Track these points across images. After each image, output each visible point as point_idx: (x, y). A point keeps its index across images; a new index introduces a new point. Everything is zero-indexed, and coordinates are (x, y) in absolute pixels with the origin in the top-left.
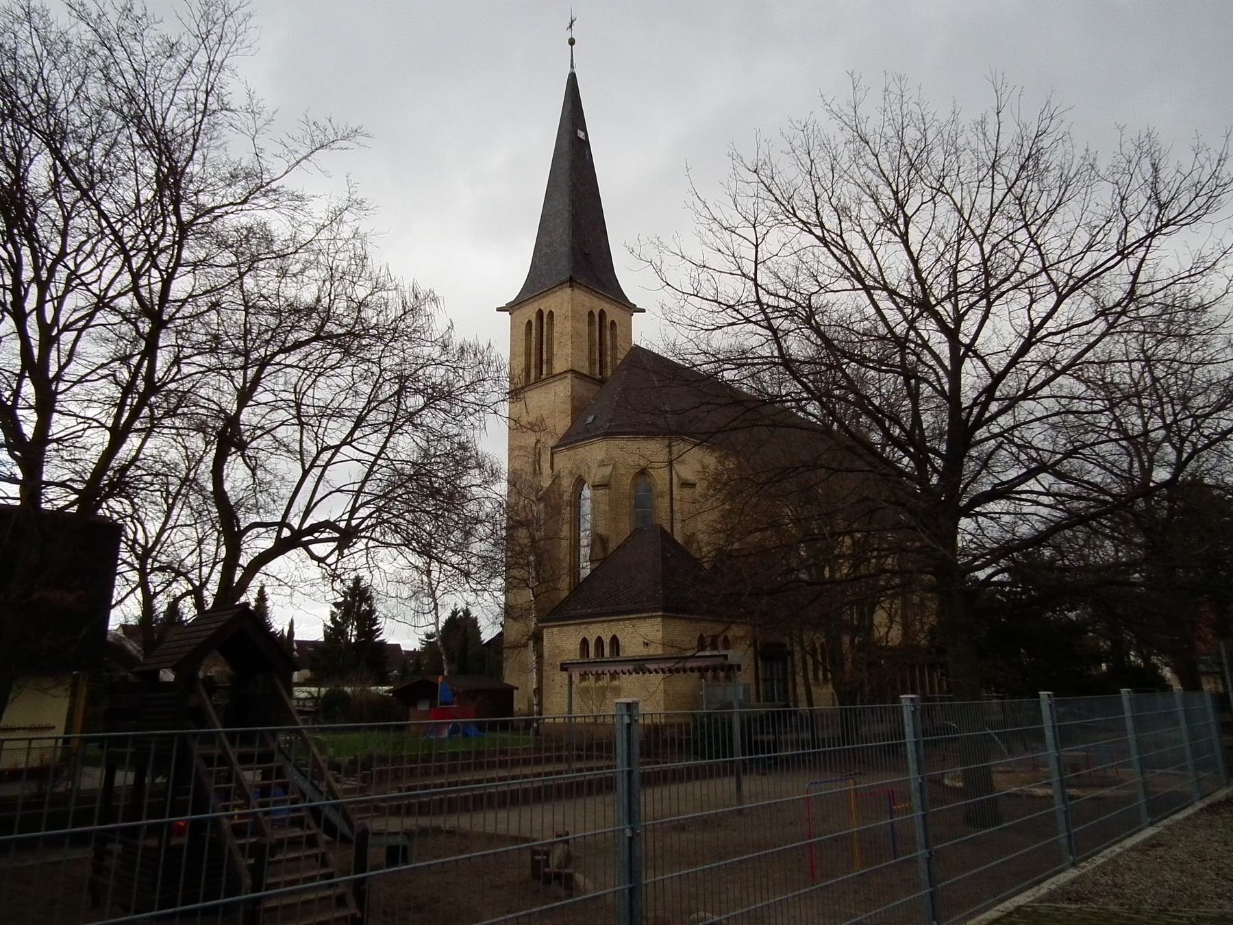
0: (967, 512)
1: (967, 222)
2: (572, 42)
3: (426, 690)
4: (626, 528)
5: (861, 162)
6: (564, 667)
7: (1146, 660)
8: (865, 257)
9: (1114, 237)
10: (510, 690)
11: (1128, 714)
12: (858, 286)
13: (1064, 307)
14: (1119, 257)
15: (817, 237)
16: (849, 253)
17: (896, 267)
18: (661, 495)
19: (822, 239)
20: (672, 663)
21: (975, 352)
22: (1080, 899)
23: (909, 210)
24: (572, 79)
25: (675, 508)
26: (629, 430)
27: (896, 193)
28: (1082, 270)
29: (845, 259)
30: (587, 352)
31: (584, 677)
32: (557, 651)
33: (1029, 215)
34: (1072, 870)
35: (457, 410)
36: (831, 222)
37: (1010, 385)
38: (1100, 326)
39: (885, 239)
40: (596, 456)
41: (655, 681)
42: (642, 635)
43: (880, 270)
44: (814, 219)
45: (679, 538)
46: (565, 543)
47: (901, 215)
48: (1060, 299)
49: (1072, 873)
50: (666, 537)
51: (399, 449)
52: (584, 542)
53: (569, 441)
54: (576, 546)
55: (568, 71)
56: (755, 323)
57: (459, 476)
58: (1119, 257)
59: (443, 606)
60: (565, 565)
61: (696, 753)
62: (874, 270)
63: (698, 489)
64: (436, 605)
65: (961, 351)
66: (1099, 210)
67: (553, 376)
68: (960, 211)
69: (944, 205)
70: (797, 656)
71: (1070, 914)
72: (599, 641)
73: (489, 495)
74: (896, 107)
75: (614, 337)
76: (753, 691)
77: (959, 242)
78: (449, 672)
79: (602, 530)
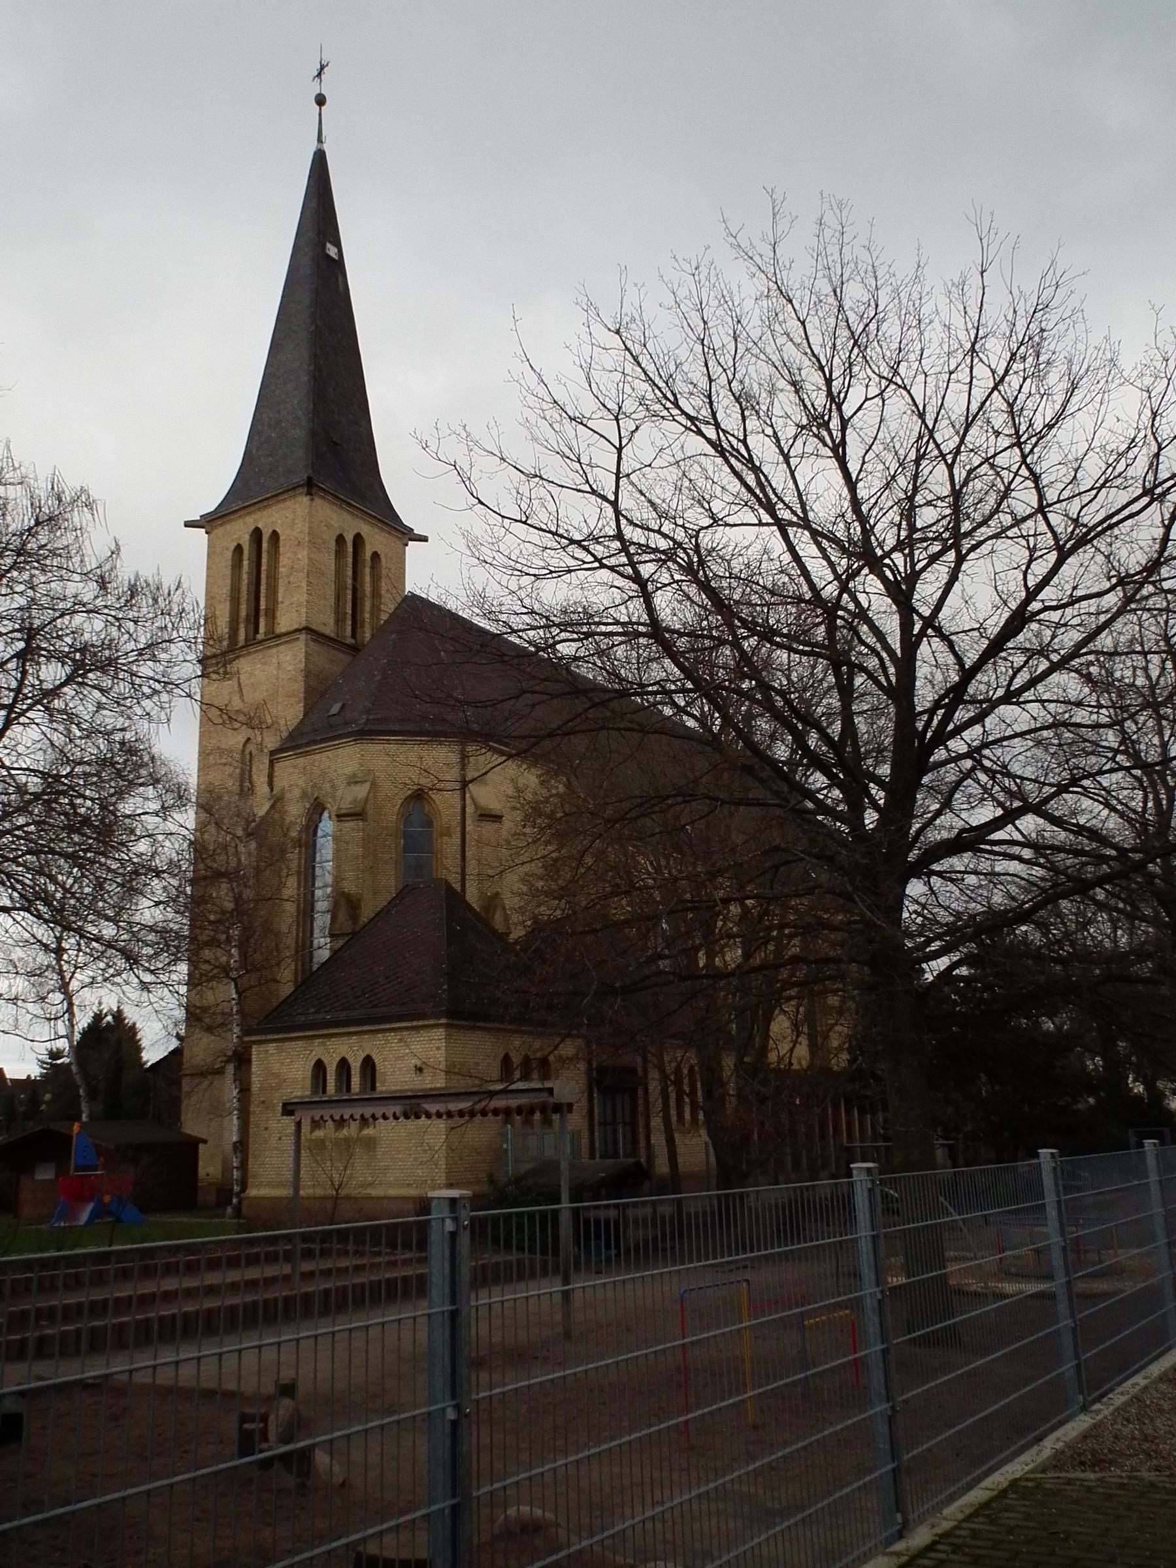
0: (921, 869)
1: (931, 433)
2: (321, 100)
3: (52, 1146)
4: (389, 882)
5: (777, 327)
6: (288, 1109)
7: (1150, 1085)
8: (778, 477)
9: (1140, 467)
10: (192, 1146)
11: (1153, 1178)
12: (766, 518)
13: (1067, 570)
14: (1146, 500)
15: (709, 441)
16: (757, 470)
17: (826, 495)
18: (447, 832)
19: (716, 445)
20: (460, 1101)
21: (939, 631)
22: (1098, 1463)
23: (848, 409)
24: (320, 165)
25: (469, 854)
26: (396, 727)
27: (829, 382)
28: (1091, 517)
29: (751, 479)
30: (332, 601)
31: (316, 1124)
32: (274, 1083)
33: (1023, 428)
34: (1082, 1417)
35: (123, 688)
36: (730, 419)
37: (985, 684)
38: (1112, 600)
39: (809, 449)
40: (343, 764)
41: (436, 1132)
42: (411, 1056)
43: (800, 496)
44: (705, 413)
45: (472, 895)
46: (290, 907)
47: (835, 414)
48: (1063, 556)
49: (1083, 1423)
50: (455, 899)
51: (20, 749)
52: (322, 906)
53: (299, 741)
54: (307, 911)
55: (313, 146)
56: (612, 569)
57: (120, 794)
58: (1146, 500)
59: (82, 1007)
60: (290, 941)
61: (496, 1241)
62: (791, 497)
63: (508, 825)
64: (71, 1005)
65: (918, 627)
66: (1119, 428)
67: (275, 637)
68: (922, 416)
69: (897, 403)
70: (654, 1086)
71: (1089, 1489)
72: (344, 1065)
73: (164, 832)
74: (833, 250)
75: (376, 578)
76: (585, 1141)
77: (917, 462)
78: (90, 1116)
79: (349, 887)
